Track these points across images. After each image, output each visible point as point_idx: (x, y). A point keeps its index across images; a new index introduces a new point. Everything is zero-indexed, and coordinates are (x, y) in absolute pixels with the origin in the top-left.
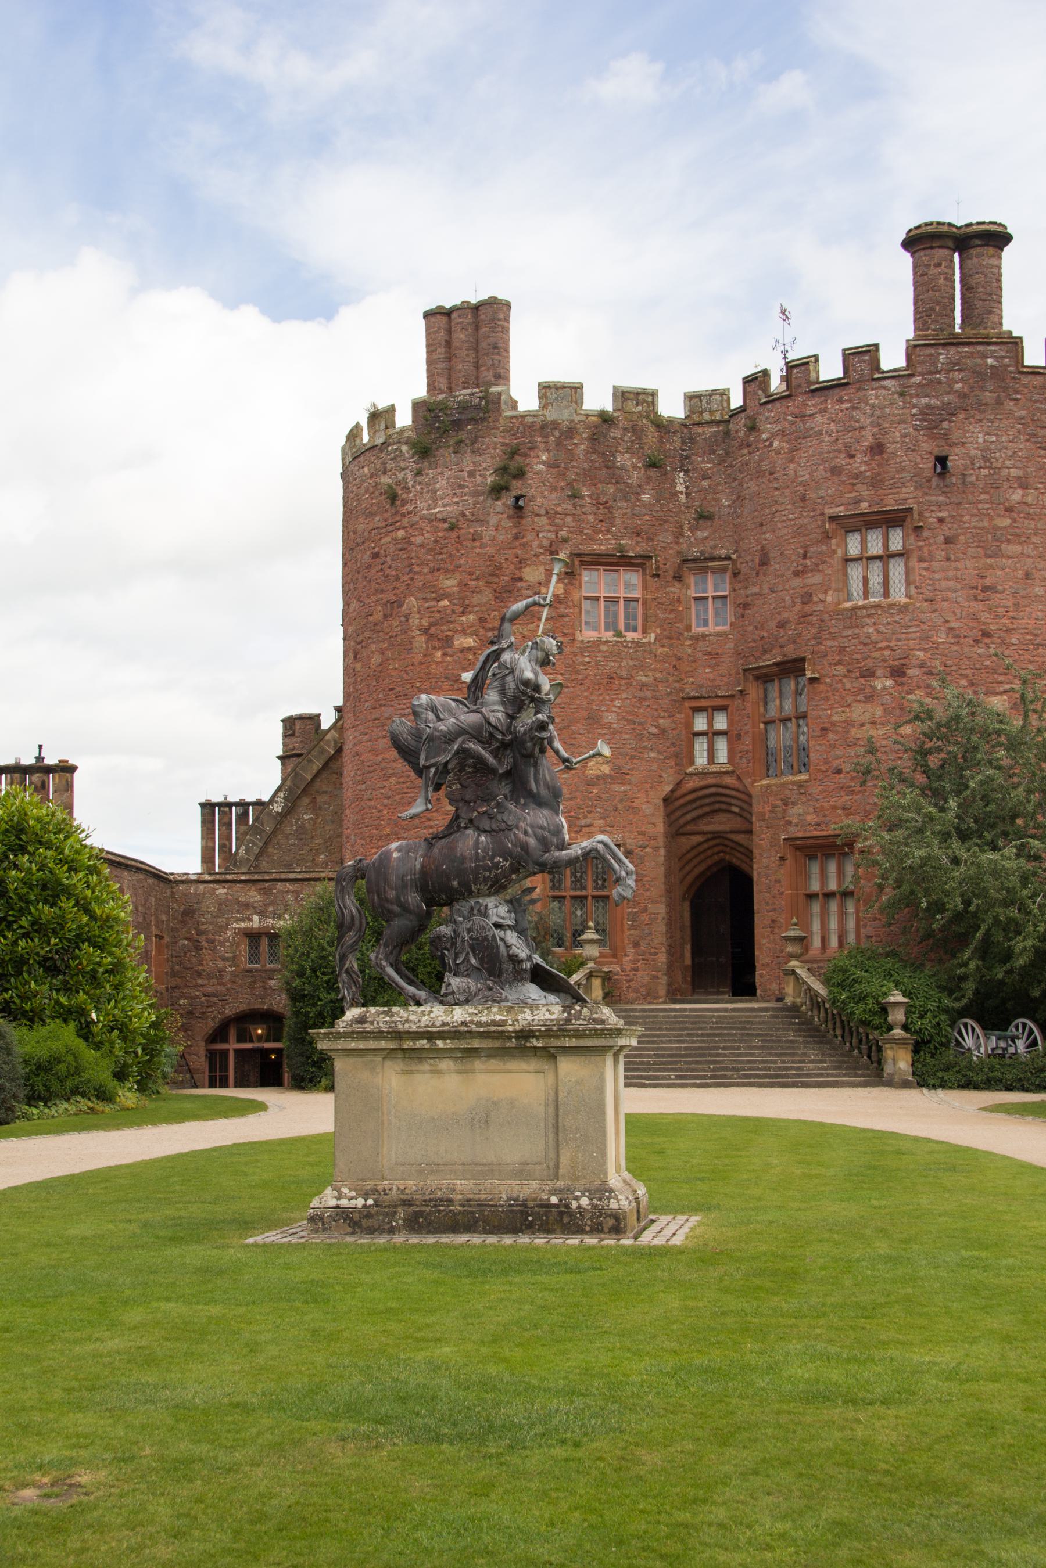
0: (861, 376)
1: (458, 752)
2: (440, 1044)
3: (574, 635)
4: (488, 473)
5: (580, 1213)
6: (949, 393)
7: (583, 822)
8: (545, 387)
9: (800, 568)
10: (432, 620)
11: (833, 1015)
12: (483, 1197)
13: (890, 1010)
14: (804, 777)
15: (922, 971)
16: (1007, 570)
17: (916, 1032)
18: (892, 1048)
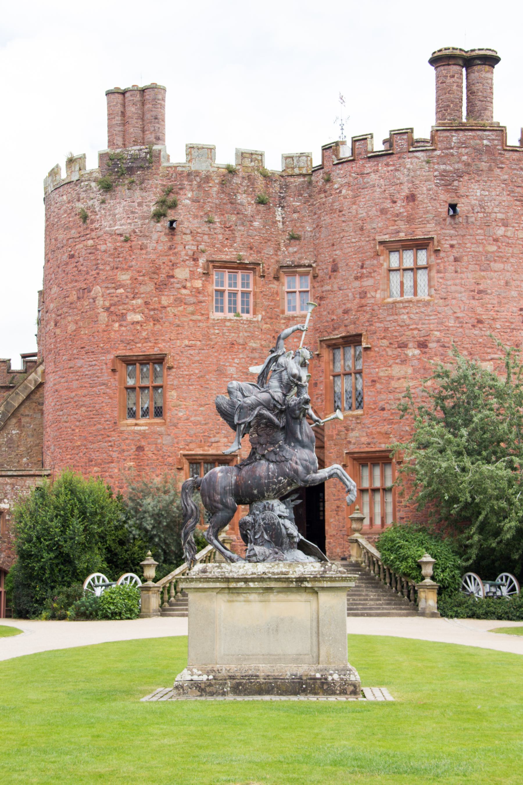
0: (401, 149)
1: (256, 416)
2: (251, 585)
3: (208, 315)
4: (152, 204)
5: (333, 683)
6: (458, 162)
7: (213, 440)
8: (191, 148)
9: (359, 274)
10: (112, 302)
11: (384, 569)
12: (276, 674)
13: (423, 567)
14: (359, 412)
15: (442, 541)
16: (494, 280)
17: (439, 581)
18: (424, 591)
